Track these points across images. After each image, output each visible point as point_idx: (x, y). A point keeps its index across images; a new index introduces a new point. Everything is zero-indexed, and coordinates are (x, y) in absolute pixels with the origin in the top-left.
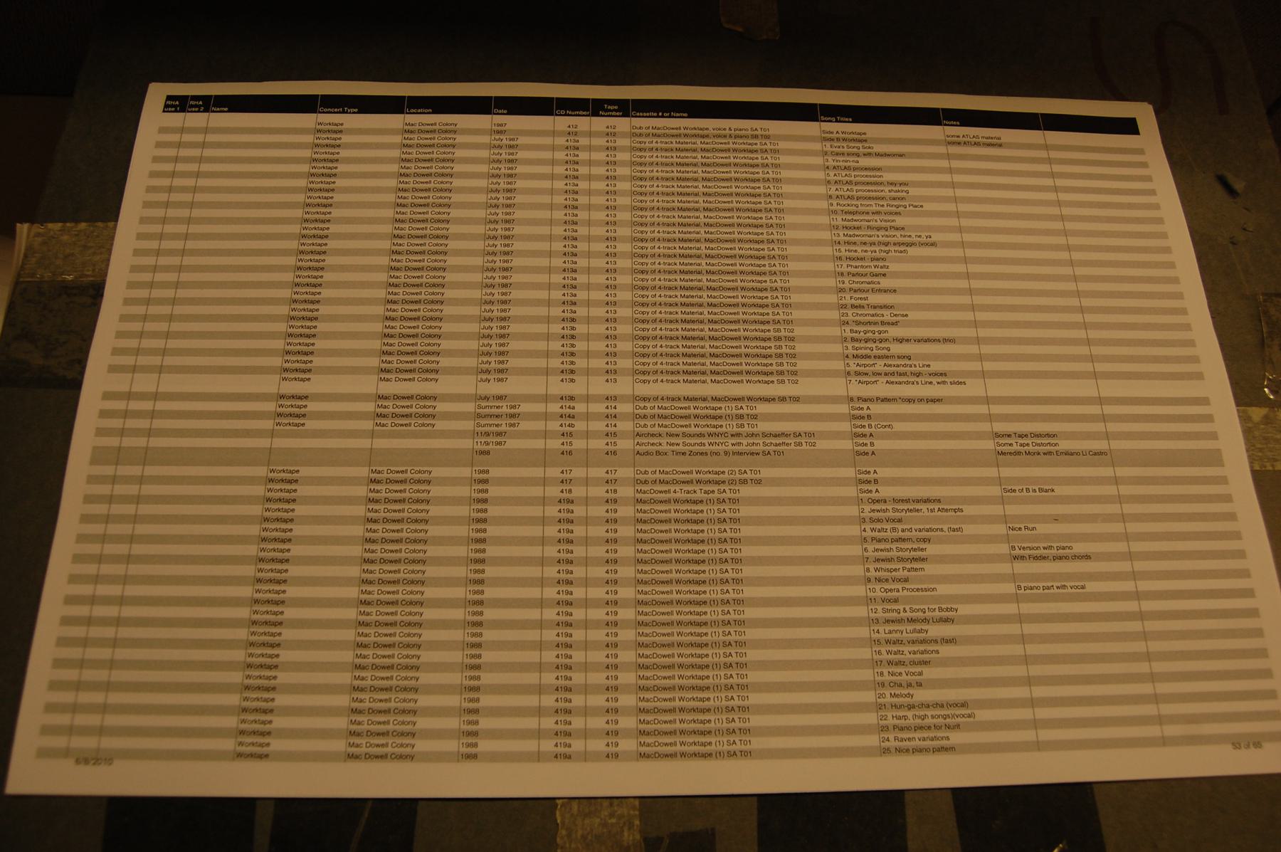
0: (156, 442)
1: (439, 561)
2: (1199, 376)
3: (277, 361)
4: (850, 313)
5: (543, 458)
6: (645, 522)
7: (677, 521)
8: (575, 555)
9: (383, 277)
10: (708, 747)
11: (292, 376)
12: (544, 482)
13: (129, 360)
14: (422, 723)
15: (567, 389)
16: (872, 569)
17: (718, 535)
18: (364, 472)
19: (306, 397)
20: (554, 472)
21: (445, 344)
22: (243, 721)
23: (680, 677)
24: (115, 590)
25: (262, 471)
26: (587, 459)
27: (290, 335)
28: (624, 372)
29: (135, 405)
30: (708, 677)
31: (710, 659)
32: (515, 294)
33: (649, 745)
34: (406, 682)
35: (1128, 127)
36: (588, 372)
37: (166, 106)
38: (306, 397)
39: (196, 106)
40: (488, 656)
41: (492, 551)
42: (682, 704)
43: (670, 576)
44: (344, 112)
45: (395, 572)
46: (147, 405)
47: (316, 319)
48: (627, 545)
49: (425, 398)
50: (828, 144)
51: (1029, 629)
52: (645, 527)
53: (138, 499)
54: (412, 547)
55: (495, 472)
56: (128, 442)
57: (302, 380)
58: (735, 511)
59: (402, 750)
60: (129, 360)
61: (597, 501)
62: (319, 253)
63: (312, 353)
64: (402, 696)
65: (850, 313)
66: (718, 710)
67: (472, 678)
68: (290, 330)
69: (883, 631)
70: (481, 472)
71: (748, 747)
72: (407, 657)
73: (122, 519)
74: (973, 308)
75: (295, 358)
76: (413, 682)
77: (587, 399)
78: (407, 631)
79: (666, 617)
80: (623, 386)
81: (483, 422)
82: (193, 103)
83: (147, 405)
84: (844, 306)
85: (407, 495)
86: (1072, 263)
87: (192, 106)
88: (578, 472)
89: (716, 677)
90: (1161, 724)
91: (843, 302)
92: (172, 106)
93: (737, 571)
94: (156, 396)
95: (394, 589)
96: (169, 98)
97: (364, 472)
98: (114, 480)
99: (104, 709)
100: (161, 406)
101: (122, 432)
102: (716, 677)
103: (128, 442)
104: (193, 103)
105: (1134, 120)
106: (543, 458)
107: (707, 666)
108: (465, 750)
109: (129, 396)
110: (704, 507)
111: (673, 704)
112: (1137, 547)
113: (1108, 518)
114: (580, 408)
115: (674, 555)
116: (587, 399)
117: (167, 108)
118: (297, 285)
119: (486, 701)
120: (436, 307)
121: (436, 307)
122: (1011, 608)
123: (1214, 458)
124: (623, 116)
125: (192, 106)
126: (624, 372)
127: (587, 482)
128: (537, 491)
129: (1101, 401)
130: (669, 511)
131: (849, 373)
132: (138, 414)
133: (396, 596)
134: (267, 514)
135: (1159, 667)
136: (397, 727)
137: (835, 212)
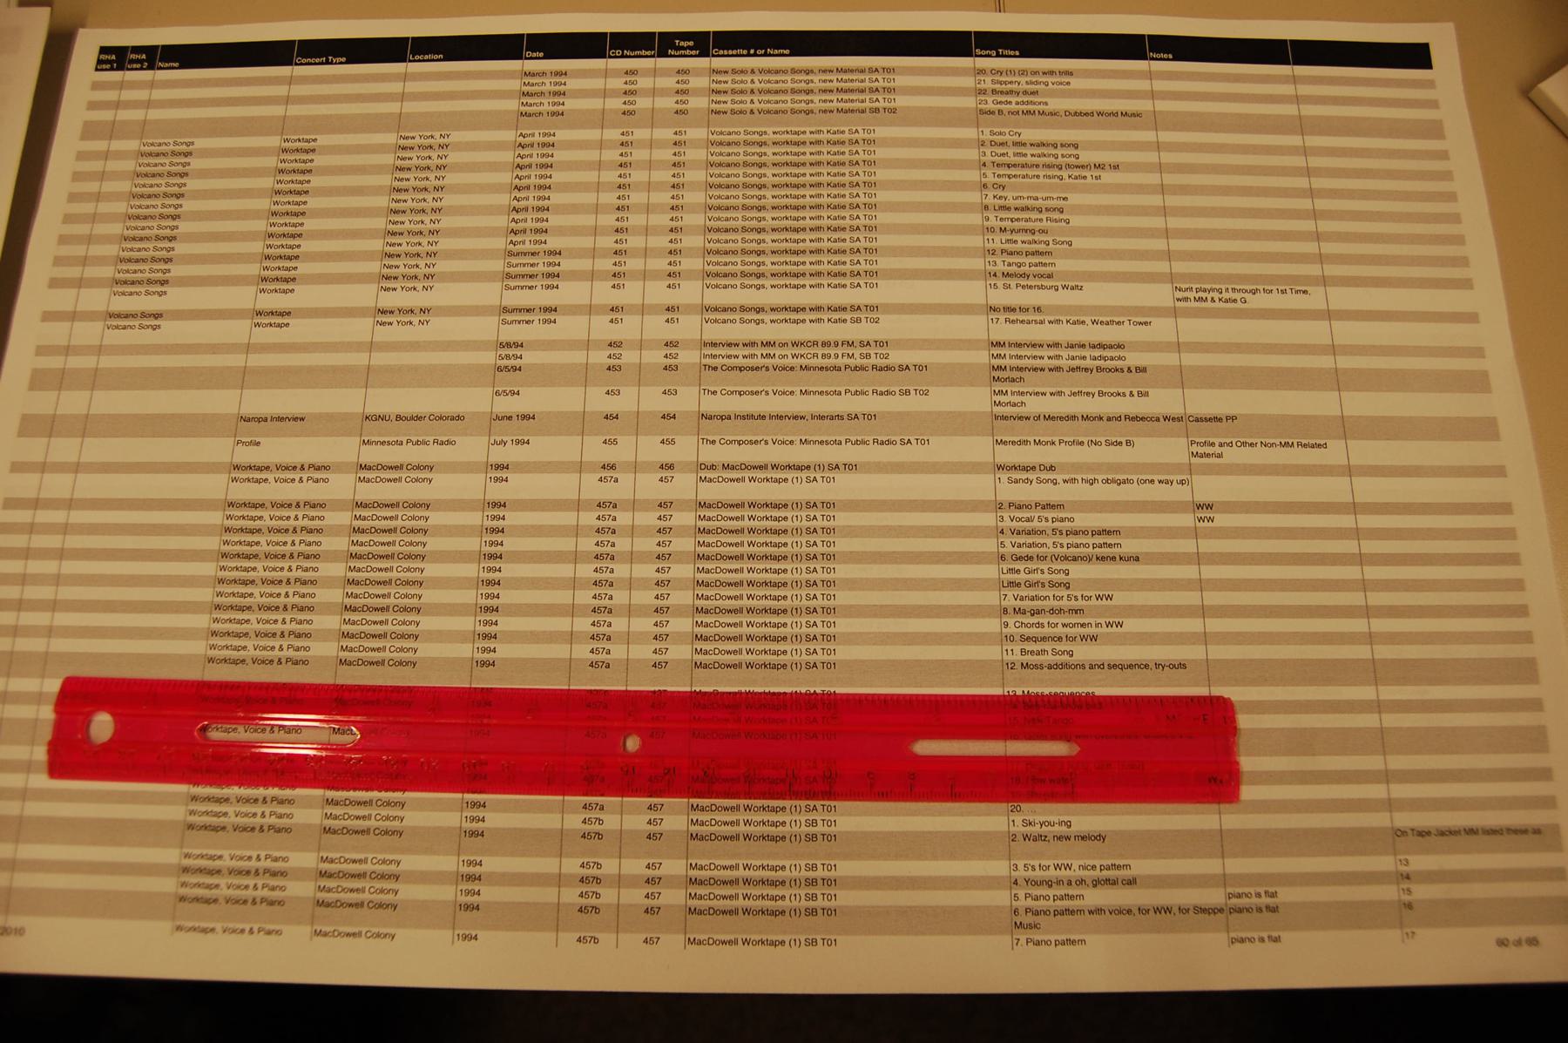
0: (107, 362)
1: (439, 583)
2: (1466, 284)
3: (254, 269)
4: (990, 100)
5: (602, 120)
6: (708, 585)
7: (750, 583)
8: (618, 522)
9: (388, 159)
10: (780, 873)
11: (244, 475)
12: (601, 145)
13: (74, 272)
14: (427, 623)
15: (608, 492)
16: (1006, 518)
17: (805, 524)
18: (391, 138)
19: (289, 314)
20: (613, 134)
21: (434, 544)
22: (192, 813)
23: (747, 823)
24: (53, 541)
25: (274, 141)
26: (653, 119)
27: (281, 171)
28: (691, 275)
29: (44, 516)
30: (785, 625)
31: (789, 601)
32: (558, 177)
33: (707, 625)
34: (381, 896)
35: (1416, 56)
36: (645, 275)
37: (100, 62)
38: (289, 314)
39: (138, 61)
40: (510, 544)
41: (510, 544)
42: (752, 524)
43: (739, 603)
44: (327, 63)
45: (391, 518)
46: (58, 516)
47: (310, 171)
48: (681, 615)
49: (414, 505)
50: (1010, 593)
51: (1210, 572)
52: (709, 513)
53: (58, 580)
54: (403, 590)
55: (491, 864)
56: (125, 115)
57: (258, 481)
58: (829, 544)
59: (383, 868)
60: (74, 272)
61: (646, 531)
62: (303, 172)
63: (310, 171)
64: (384, 812)
65: (990, 100)
66: (797, 611)
67: (486, 623)
68: (275, 208)
69: (998, 242)
70: (470, 863)
71: (832, 630)
72: (404, 623)
73: (49, 529)
74: (1167, 233)
75: (289, 178)
76: (415, 601)
77: (634, 505)
78: (408, 539)
79: (727, 902)
80: (689, 292)
81: (514, 261)
82: (133, 56)
83: (58, 516)
84: (983, 92)
85: (366, 896)
86: (1318, 237)
87: (132, 61)
88: (641, 134)
89: (794, 597)
90: (1388, 782)
91: (982, 86)
92: (107, 62)
93: (830, 823)
94: (70, 504)
95: (385, 591)
96: (104, 50)
97: (391, 138)
98: (106, 155)
99: (65, 529)
100: (78, 517)
101: (117, 105)
102: (795, 625)
103: (125, 115)
104: (133, 56)
105: (1426, 46)
106: (602, 120)
107: (785, 611)
108: (482, 629)
109: (36, 504)
110: (787, 647)
111: (738, 630)
112: (1315, 162)
113: (1340, 534)
114: (623, 518)
115: (747, 523)
116: (634, 505)
117: (101, 65)
118: (278, 192)
119: (506, 624)
120: (419, 513)
121: (419, 513)
122: (1188, 546)
123: (1435, 130)
124: (699, 56)
125: (132, 61)
126: (691, 275)
127: (651, 144)
128: (591, 176)
129: (1354, 508)
130: (737, 823)
131: (985, 186)
132: (44, 554)
133: (387, 601)
134: (226, 548)
135: (1369, 547)
136: (374, 897)
137: (991, 230)
